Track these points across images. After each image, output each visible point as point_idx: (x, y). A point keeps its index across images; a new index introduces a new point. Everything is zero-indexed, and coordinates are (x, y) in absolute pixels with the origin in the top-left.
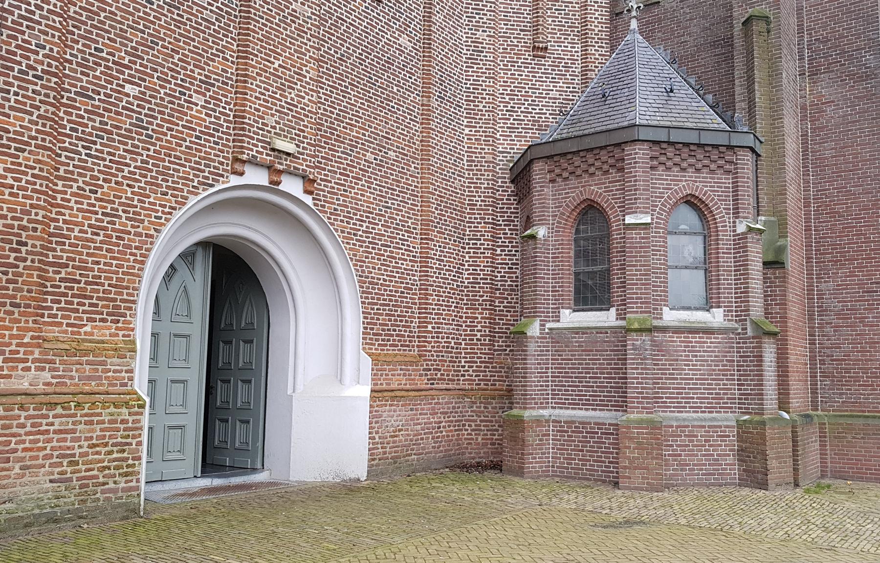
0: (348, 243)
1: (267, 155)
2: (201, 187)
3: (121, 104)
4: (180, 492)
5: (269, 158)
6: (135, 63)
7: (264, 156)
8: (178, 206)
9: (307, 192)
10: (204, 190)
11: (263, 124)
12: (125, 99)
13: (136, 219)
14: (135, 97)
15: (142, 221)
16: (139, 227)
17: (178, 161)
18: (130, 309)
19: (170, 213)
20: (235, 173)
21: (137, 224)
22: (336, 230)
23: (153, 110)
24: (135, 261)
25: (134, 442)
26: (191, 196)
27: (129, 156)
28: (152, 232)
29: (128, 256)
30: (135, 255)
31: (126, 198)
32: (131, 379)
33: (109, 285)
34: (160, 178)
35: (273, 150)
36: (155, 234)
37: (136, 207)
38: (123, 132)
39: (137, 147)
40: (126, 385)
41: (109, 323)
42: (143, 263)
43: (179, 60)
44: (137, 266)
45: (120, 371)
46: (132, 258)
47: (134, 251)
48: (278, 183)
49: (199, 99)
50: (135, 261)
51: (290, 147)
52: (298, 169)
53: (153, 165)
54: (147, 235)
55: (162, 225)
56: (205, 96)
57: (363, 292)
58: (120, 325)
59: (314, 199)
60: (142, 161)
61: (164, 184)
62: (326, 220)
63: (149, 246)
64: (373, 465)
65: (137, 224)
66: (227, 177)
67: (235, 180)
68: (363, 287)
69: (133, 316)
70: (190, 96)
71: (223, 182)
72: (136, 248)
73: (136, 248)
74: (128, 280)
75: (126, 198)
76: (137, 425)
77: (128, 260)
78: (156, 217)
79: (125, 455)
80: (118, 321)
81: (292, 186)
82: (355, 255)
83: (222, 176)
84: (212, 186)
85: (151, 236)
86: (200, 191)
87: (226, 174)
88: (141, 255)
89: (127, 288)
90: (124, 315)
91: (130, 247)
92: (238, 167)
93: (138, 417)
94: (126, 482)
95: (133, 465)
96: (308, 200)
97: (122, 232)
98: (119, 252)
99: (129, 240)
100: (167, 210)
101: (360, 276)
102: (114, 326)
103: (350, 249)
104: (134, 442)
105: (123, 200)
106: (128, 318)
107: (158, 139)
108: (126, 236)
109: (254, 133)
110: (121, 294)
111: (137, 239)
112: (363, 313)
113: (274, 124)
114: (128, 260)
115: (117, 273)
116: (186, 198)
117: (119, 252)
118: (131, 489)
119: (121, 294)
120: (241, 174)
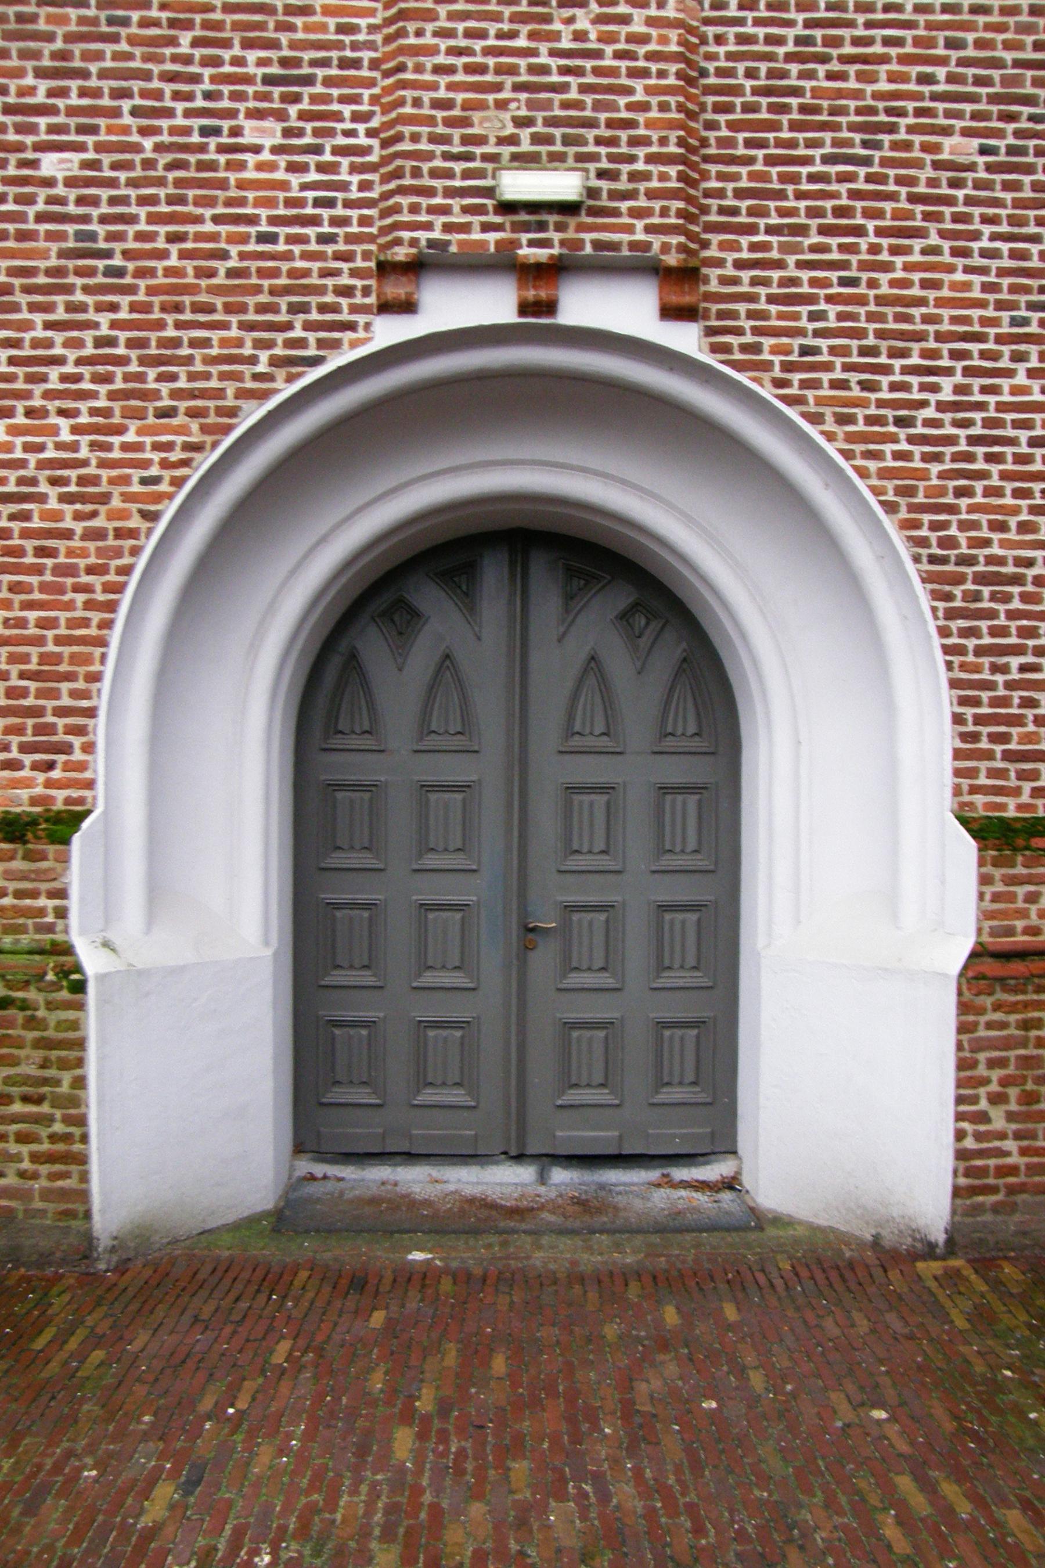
0: (870, 455)
1: (486, 228)
2: (281, 374)
3: (31, 211)
4: (701, 1159)
5: (492, 237)
6: (63, 93)
7: (476, 236)
8: (209, 439)
9: (670, 312)
10: (290, 379)
11: (466, 140)
12: (42, 193)
13: (88, 497)
14: (70, 182)
15: (104, 498)
16: (94, 514)
17: (202, 318)
18: (80, 731)
19: (185, 463)
20: (385, 308)
21: (89, 508)
22: (815, 419)
23: (124, 201)
24: (89, 605)
25: (67, 1078)
26: (246, 405)
27: (59, 337)
28: (135, 522)
29: (69, 596)
30: (87, 589)
31: (59, 446)
32: (62, 913)
33: (22, 675)
34: (152, 373)
35: (508, 208)
36: (144, 525)
37: (85, 463)
38: (42, 280)
39: (82, 308)
40: (50, 928)
41: (26, 773)
42: (111, 607)
43: (196, 43)
44: (96, 617)
45: (34, 894)
46: (80, 598)
47: (85, 579)
48: (550, 307)
49: (262, 131)
50: (89, 605)
51: (562, 184)
52: (614, 246)
53: (131, 344)
54: (119, 534)
55: (159, 497)
56: (281, 116)
57: (951, 614)
58: (56, 774)
59: (710, 332)
60: (100, 342)
61: (165, 388)
62: (767, 393)
63: (126, 560)
64: (978, 1209)
65: (89, 508)
66: (367, 326)
67: (389, 332)
68: (949, 597)
69: (89, 748)
70: (236, 132)
71: (354, 344)
72: (90, 570)
73: (90, 570)
74: (73, 656)
75: (59, 446)
76: (71, 1035)
77: (69, 606)
78: (144, 481)
79: (45, 1108)
80: (50, 766)
81: (622, 308)
82: (907, 492)
83: (351, 327)
84: (315, 362)
85: (133, 534)
86: (279, 384)
87: (361, 319)
88: (108, 588)
89: (70, 677)
90: (65, 749)
91: (70, 571)
92: (396, 290)
93: (71, 1015)
94: (53, 1177)
95: (67, 1138)
96: (685, 339)
97: (49, 534)
98: (44, 587)
99: (70, 553)
100: (175, 456)
101: (933, 559)
102: (41, 777)
103: (885, 474)
104: (67, 1078)
105: (50, 454)
106: (78, 755)
107: (140, 273)
108: (61, 545)
109: (434, 174)
110: (55, 694)
111: (92, 546)
112: (954, 684)
113: (510, 130)
114: (69, 606)
115: (40, 641)
116: (232, 412)
117: (44, 587)
118: (64, 1194)
119: (55, 694)
120: (408, 307)
